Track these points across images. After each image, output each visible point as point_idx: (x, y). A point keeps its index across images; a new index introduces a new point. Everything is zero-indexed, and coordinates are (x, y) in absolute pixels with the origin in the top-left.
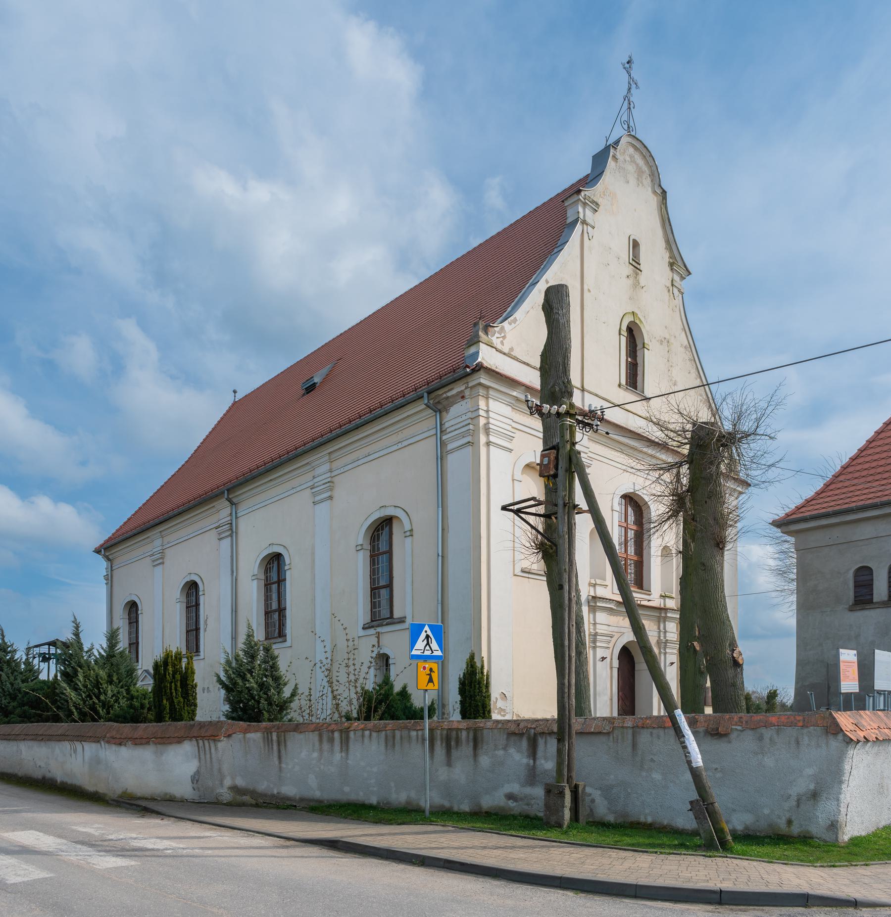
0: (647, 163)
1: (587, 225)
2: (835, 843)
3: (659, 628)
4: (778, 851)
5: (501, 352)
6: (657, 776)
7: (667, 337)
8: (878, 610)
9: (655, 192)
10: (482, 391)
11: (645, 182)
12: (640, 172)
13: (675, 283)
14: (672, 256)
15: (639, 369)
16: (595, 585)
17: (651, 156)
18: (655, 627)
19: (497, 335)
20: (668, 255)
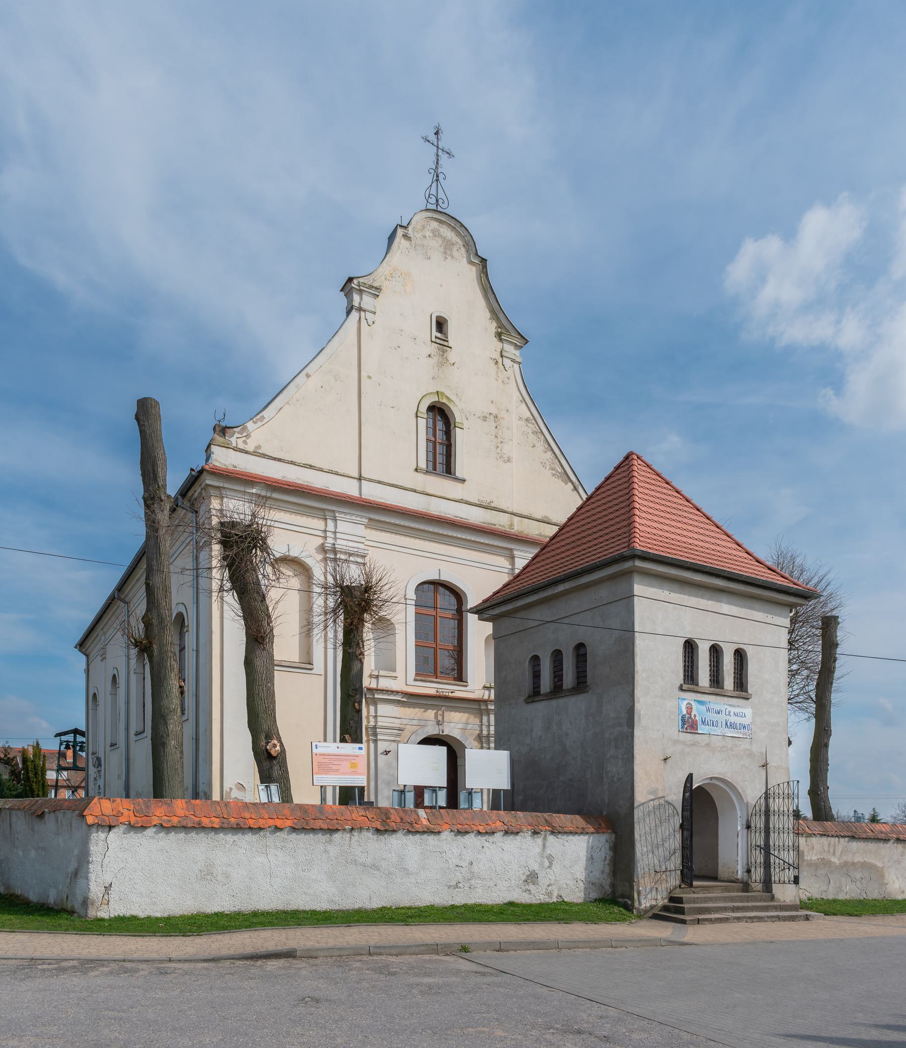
0: (458, 234)
1: (365, 311)
2: (83, 917)
3: (481, 722)
4: (47, 920)
5: (247, 452)
6: (20, 853)
7: (494, 412)
8: (544, 702)
9: (471, 262)
10: (213, 492)
11: (455, 254)
12: (448, 246)
13: (504, 354)
14: (500, 325)
15: (453, 449)
16: (377, 677)
17: (462, 225)
18: (477, 721)
19: (236, 435)
20: (494, 324)
